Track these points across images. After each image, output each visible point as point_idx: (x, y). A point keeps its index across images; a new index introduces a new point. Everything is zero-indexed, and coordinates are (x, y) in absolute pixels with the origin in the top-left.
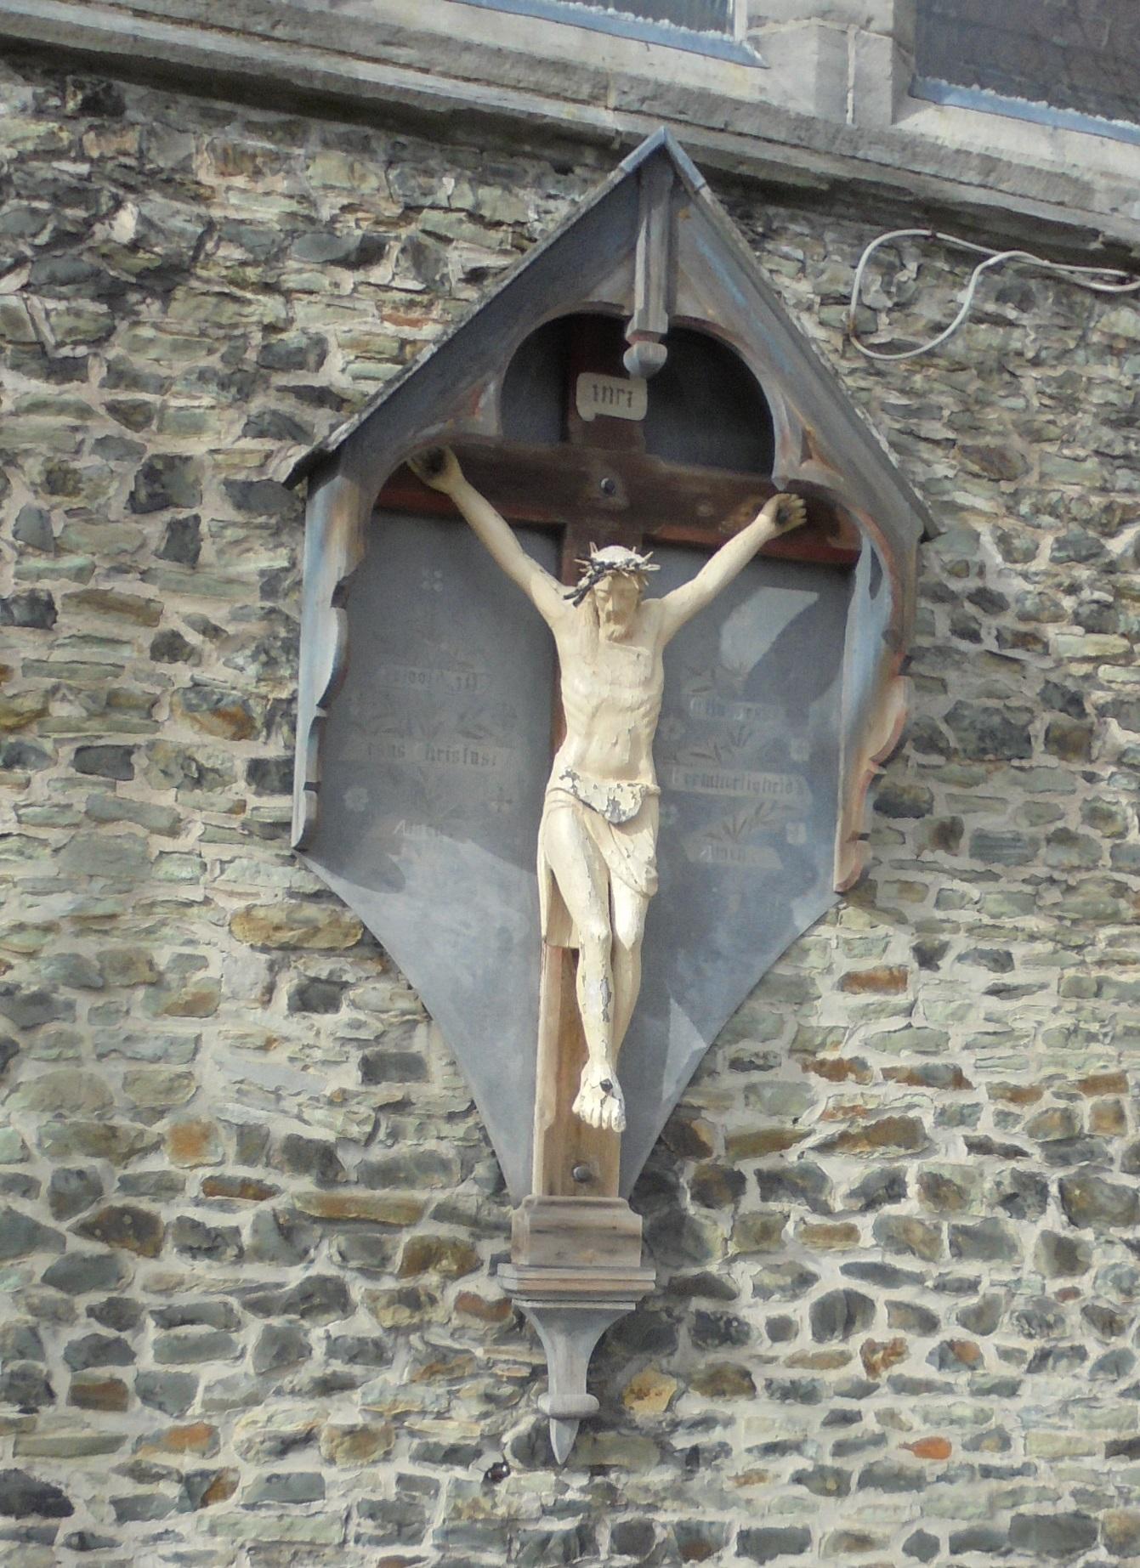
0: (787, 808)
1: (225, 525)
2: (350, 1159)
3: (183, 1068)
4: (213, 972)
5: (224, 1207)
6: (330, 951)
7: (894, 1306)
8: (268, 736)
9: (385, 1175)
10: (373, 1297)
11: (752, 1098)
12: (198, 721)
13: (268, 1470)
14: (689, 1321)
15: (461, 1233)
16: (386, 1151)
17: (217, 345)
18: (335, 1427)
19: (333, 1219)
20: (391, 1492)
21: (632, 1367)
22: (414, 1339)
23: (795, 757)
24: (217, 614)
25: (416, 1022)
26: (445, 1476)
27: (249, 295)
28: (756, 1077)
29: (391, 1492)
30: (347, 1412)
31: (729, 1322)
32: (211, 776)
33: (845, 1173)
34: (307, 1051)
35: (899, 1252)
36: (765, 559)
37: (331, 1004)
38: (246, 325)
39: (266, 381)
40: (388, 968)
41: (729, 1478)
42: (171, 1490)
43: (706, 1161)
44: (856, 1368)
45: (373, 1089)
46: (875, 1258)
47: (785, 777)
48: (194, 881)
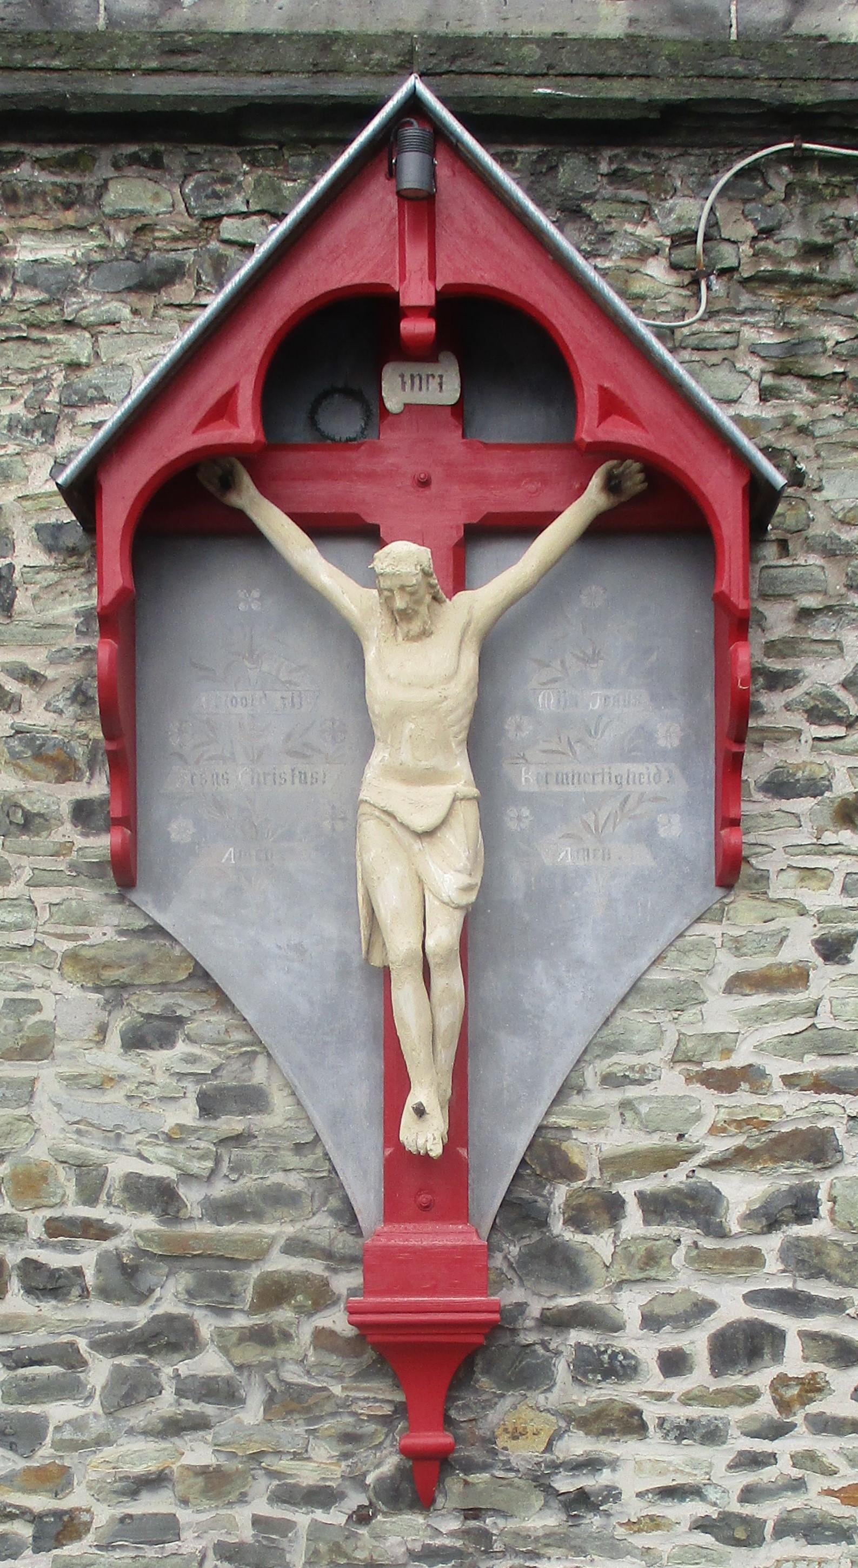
0: (656, 799)
1: (38, 569)
2: (192, 1196)
3: (23, 1111)
4: (47, 1015)
5: (68, 1248)
6: (163, 987)
7: (808, 1337)
8: (92, 775)
9: (233, 1209)
10: (220, 1333)
11: (629, 1115)
12: (21, 768)
13: (120, 1511)
14: (568, 1353)
15: (316, 1267)
16: (232, 1185)
17: (19, 391)
18: (188, 1468)
19: (176, 1256)
20: (247, 1534)
21: (505, 1404)
22: (270, 1376)
23: (662, 743)
24: (35, 659)
25: (255, 1053)
26: (302, 1518)
27: (50, 337)
28: (632, 1092)
29: (247, 1534)
30: (198, 1452)
31: (614, 1356)
32: (38, 820)
33: (741, 1192)
34: (145, 1088)
35: (812, 1276)
36: (598, 532)
37: (166, 1040)
38: (47, 367)
39: (72, 419)
40: (224, 1002)
41: (621, 1525)
42: (24, 1530)
43: (577, 1184)
44: (765, 1407)
45: (212, 1124)
46: (785, 1284)
47: (652, 768)
48: (21, 927)
